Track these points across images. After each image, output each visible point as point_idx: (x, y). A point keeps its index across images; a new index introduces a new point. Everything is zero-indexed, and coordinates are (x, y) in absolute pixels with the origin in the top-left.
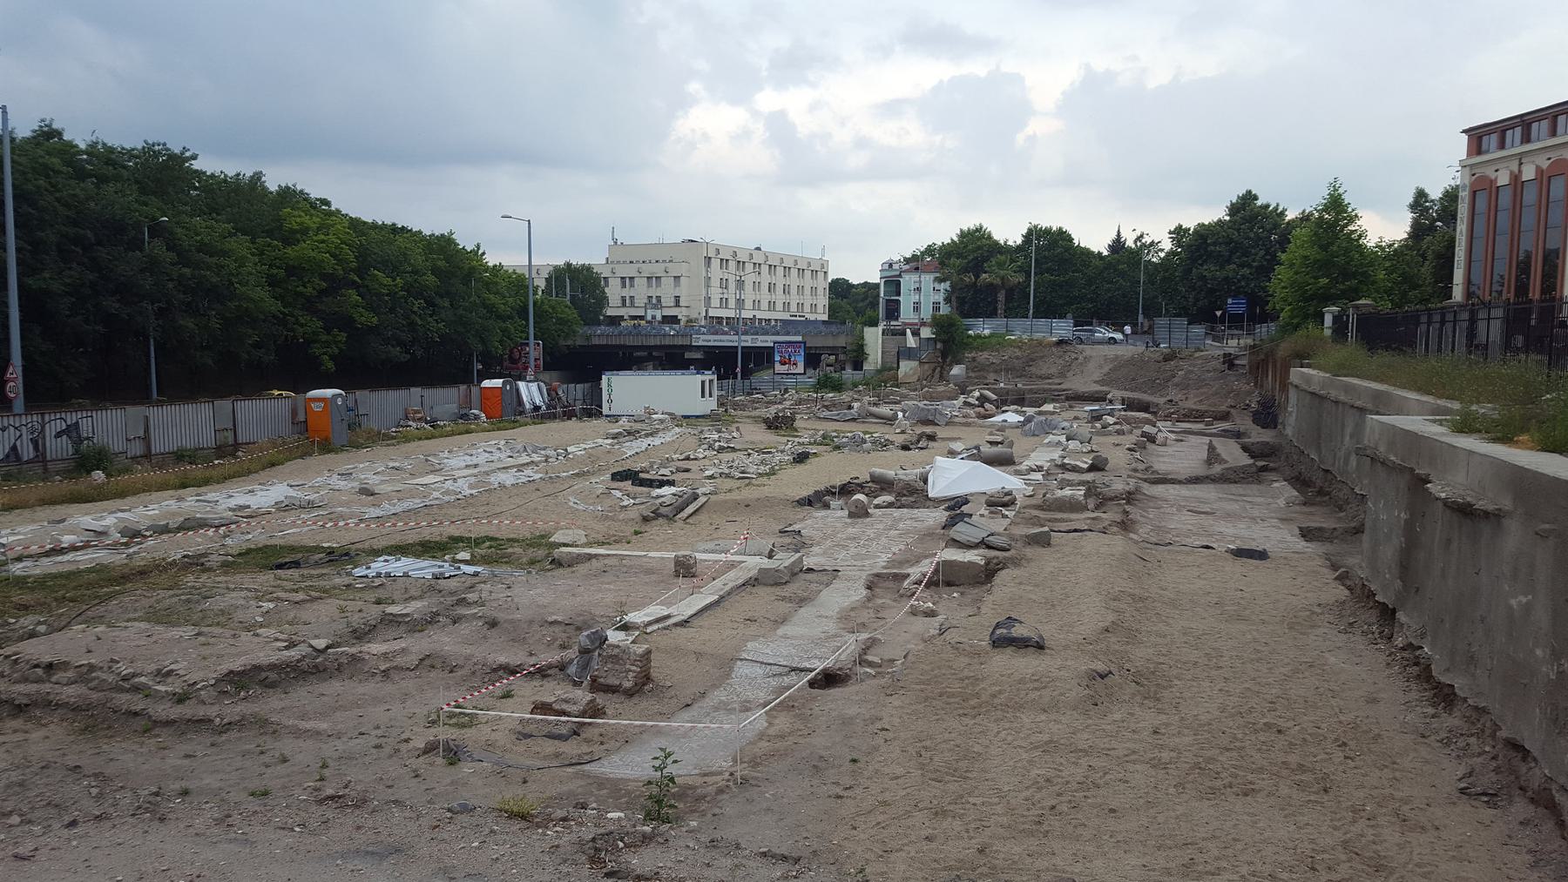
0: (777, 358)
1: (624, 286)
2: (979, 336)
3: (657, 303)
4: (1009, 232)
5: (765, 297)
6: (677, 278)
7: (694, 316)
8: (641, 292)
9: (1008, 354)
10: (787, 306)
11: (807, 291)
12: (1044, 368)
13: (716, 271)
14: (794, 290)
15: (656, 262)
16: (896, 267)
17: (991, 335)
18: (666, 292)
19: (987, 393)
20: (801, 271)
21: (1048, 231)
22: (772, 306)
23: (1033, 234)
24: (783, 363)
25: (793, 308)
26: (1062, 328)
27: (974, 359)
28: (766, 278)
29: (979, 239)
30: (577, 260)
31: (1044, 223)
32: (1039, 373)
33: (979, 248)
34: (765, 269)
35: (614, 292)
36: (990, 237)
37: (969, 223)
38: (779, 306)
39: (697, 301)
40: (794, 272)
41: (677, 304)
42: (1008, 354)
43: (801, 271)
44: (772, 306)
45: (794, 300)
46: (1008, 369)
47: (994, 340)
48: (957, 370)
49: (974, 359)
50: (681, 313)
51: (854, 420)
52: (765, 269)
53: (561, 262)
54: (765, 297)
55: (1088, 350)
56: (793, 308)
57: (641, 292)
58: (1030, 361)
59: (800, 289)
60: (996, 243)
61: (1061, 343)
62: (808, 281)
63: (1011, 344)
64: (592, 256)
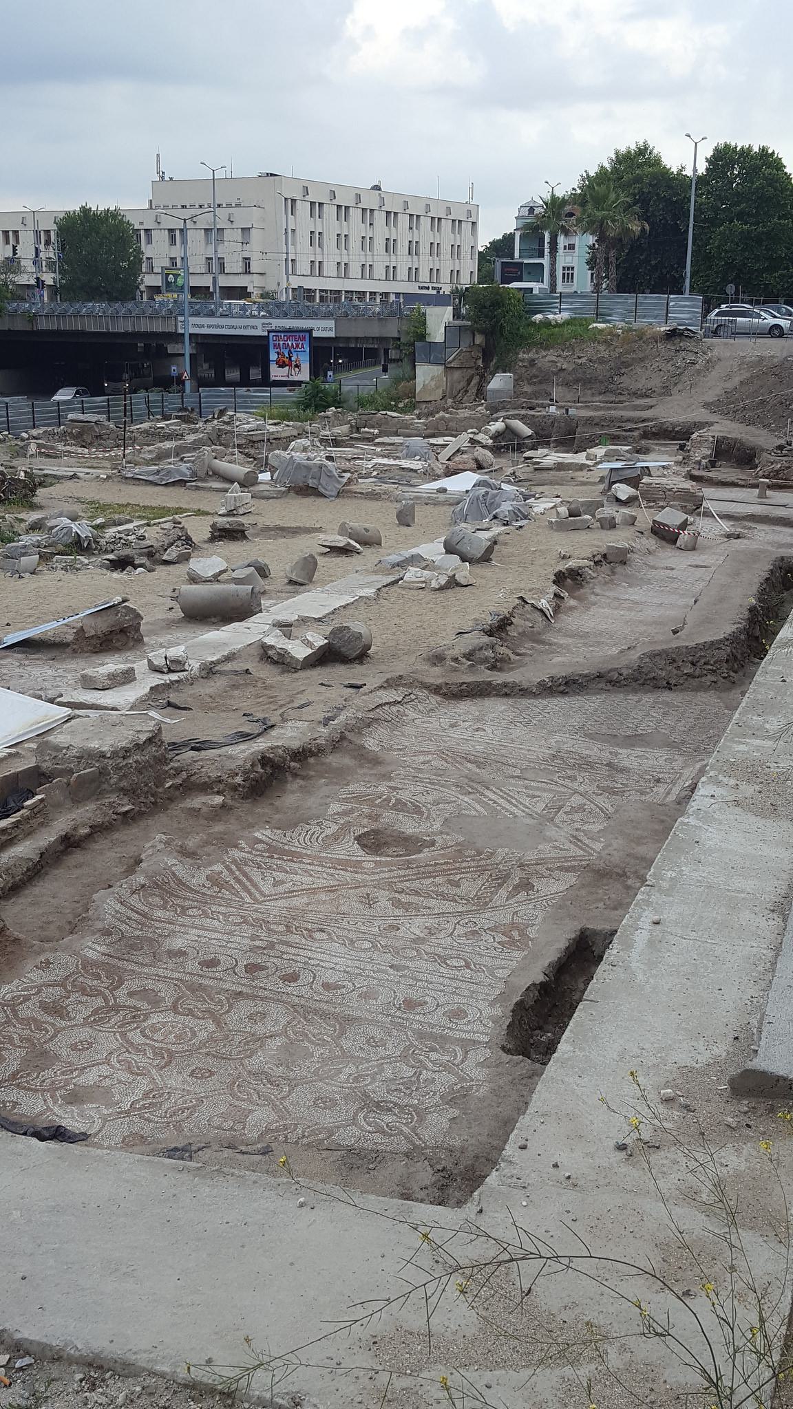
0: (273, 356)
1: (173, 241)
2: (547, 324)
3: (216, 265)
4: (684, 156)
5: (380, 260)
6: (245, 230)
7: (271, 287)
8: (197, 250)
9: (589, 351)
10: (413, 273)
11: (403, 248)
12: (643, 378)
13: (303, 221)
14: (424, 249)
15: (208, 207)
16: (537, 211)
17: (567, 323)
18: (231, 253)
19: (518, 425)
20: (436, 221)
21: (745, 153)
22: (391, 273)
23: (723, 158)
24: (281, 365)
25: (424, 276)
26: (684, 309)
27: (532, 362)
28: (381, 231)
29: (640, 166)
30: (99, 204)
31: (740, 142)
32: (633, 387)
33: (638, 180)
34: (380, 218)
35: (157, 252)
36: (658, 161)
37: (628, 143)
38: (402, 273)
39: (282, 262)
40: (425, 223)
41: (247, 271)
42: (589, 351)
43: (414, 219)
44: (391, 273)
45: (425, 263)
46: (583, 380)
47: (567, 331)
48: (499, 382)
49: (532, 362)
50: (252, 284)
51: (181, 483)
52: (380, 218)
53: (75, 207)
54: (380, 260)
55: (720, 347)
56: (424, 276)
57: (197, 250)
58: (622, 366)
59: (435, 248)
60: (665, 172)
61: (673, 334)
62: (446, 237)
63: (596, 337)
64: (128, 198)
